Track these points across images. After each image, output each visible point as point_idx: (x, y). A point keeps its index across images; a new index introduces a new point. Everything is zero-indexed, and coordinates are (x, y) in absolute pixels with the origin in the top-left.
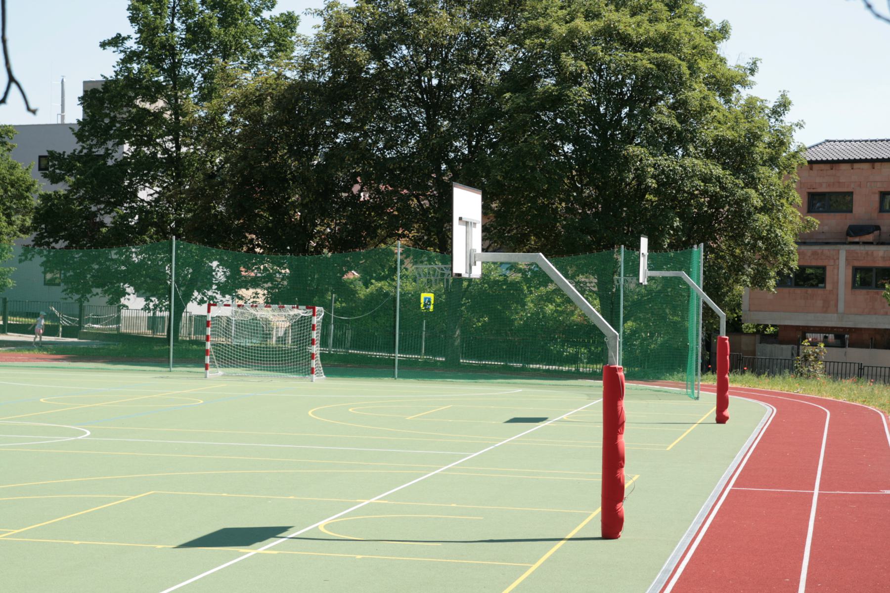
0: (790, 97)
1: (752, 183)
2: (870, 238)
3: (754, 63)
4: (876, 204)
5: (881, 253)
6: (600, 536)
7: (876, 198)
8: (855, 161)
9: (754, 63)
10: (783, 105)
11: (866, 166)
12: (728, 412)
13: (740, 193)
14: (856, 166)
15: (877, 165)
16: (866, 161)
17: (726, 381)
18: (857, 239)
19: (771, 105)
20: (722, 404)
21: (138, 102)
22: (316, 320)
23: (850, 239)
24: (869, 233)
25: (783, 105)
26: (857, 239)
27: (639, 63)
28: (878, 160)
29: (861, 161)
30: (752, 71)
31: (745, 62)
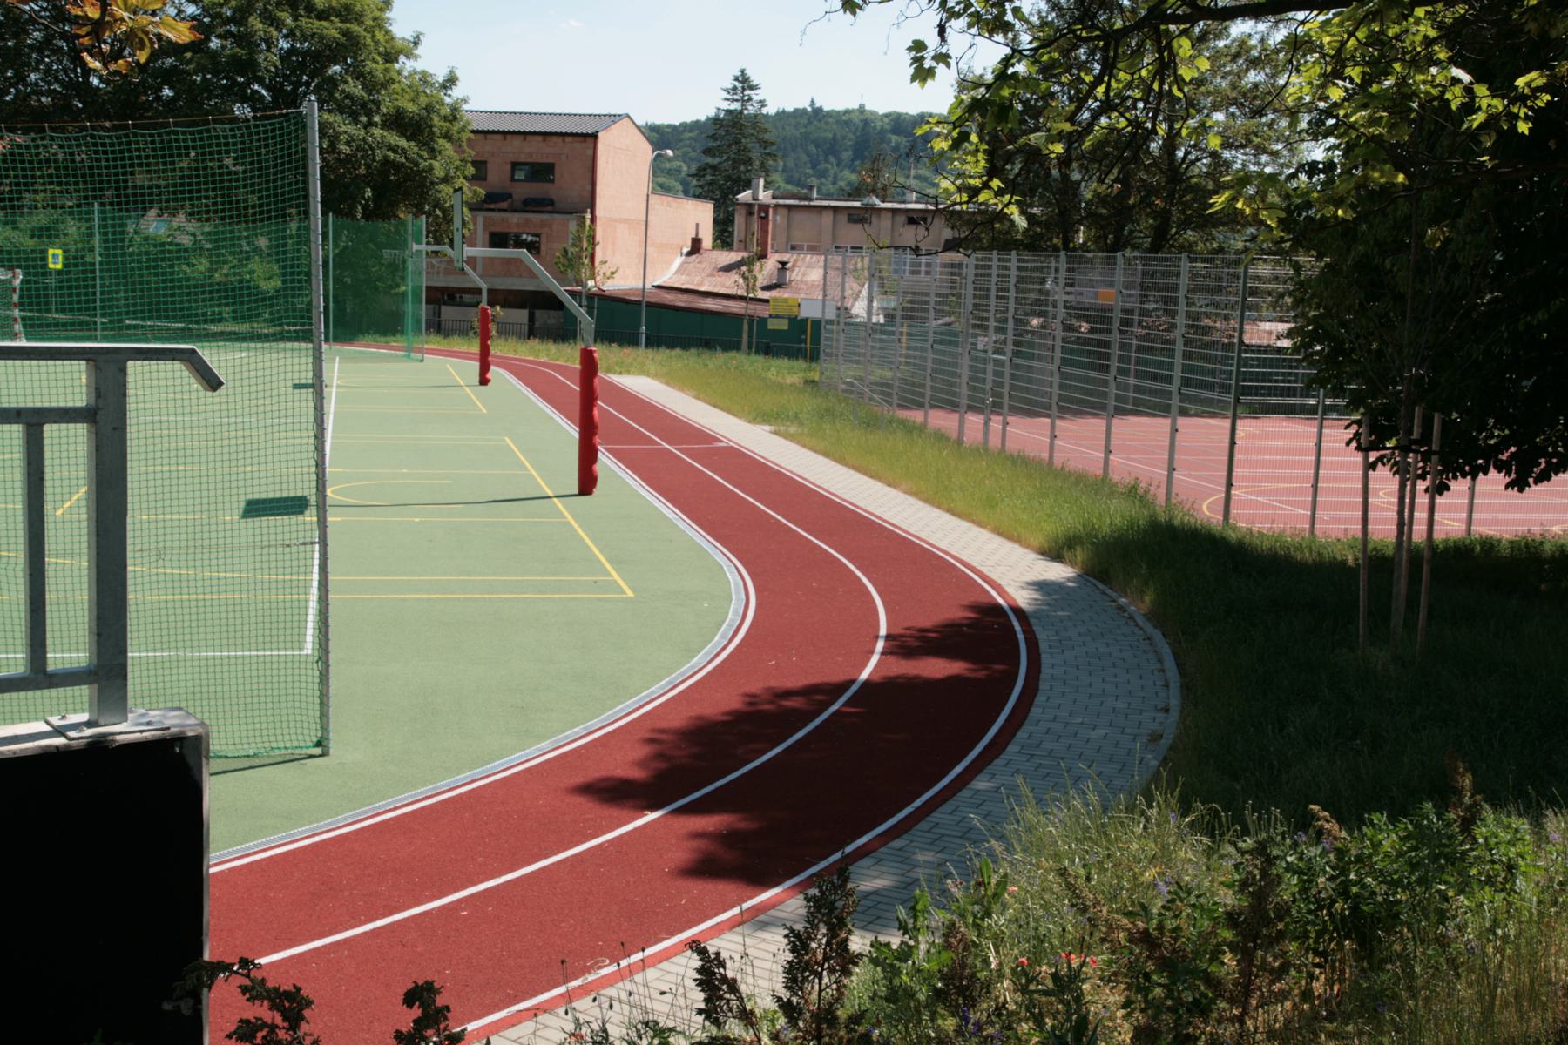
0: (458, 73)
1: (433, 153)
2: (504, 205)
3: (418, 37)
4: (508, 174)
5: (515, 220)
6: (576, 492)
7: (509, 167)
8: (488, 132)
9: (418, 37)
10: (451, 81)
11: (499, 137)
12: (489, 375)
13: (423, 164)
14: (489, 136)
15: (509, 137)
16: (498, 132)
17: (488, 347)
18: (492, 206)
19: (441, 80)
20: (484, 368)
21: (1021, 222)
22: (17, 283)
23: (486, 206)
24: (504, 201)
25: (451, 81)
26: (492, 206)
27: (325, 31)
28: (509, 133)
29: (493, 132)
30: (416, 44)
31: (409, 35)
